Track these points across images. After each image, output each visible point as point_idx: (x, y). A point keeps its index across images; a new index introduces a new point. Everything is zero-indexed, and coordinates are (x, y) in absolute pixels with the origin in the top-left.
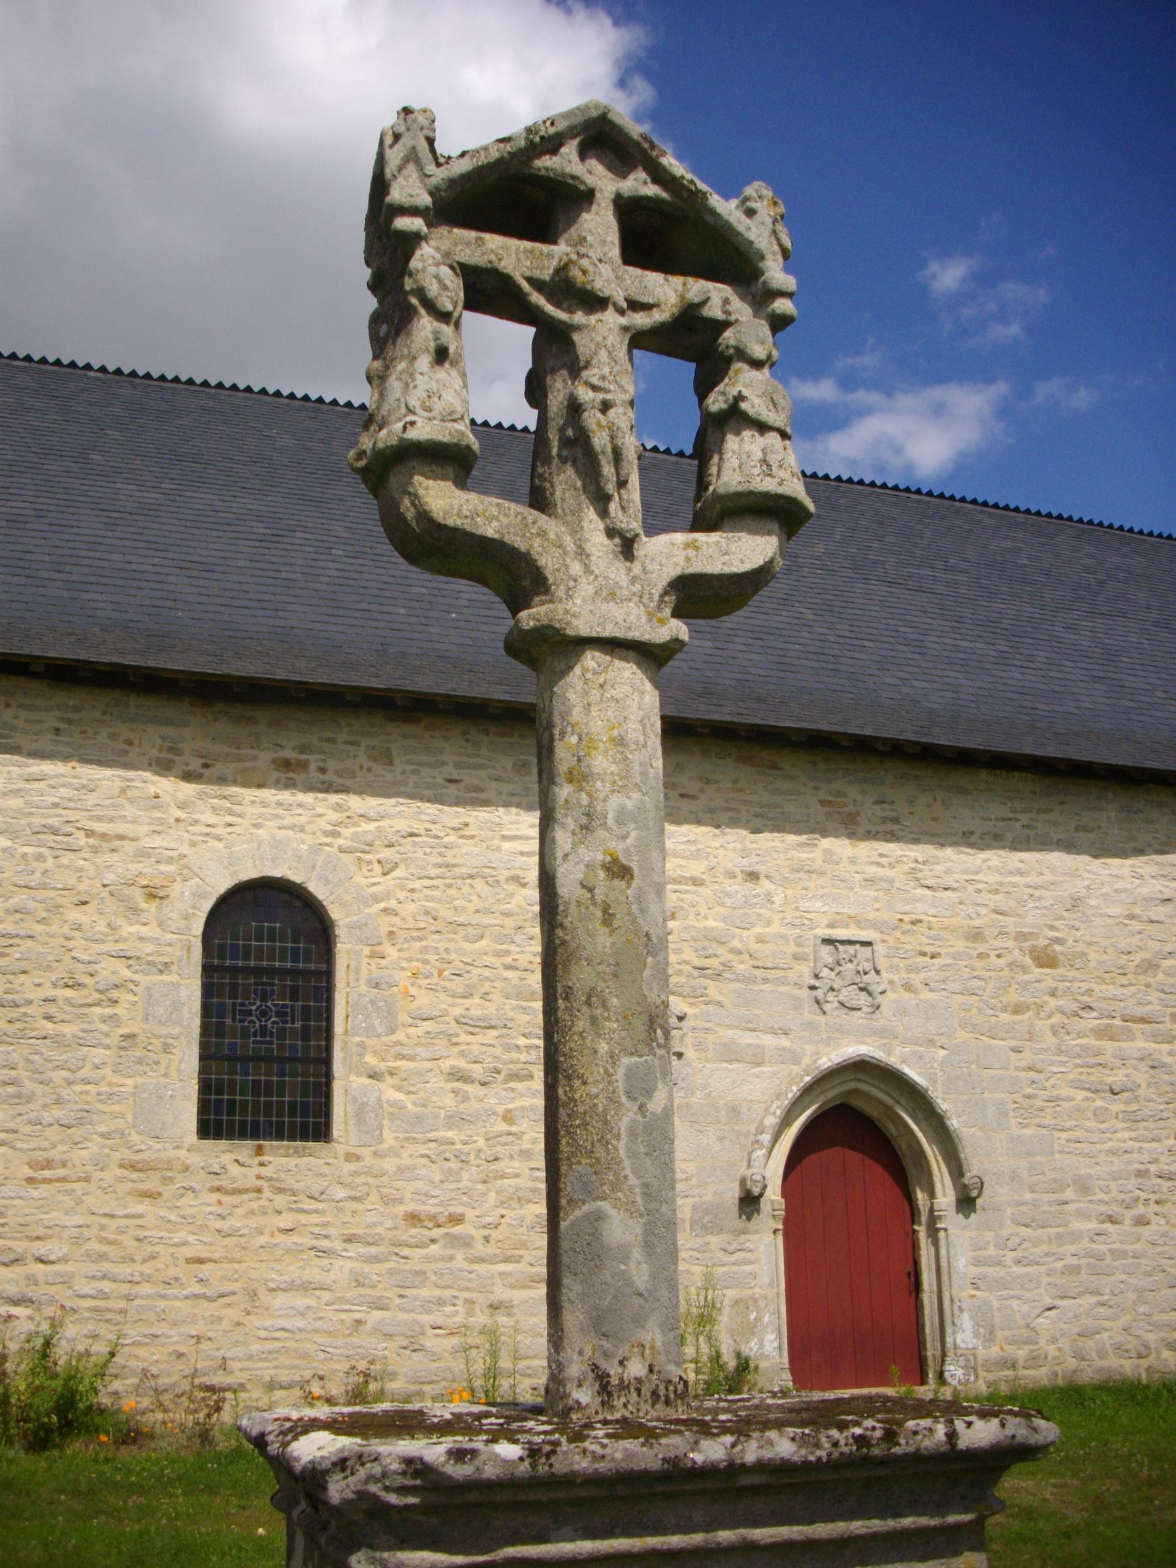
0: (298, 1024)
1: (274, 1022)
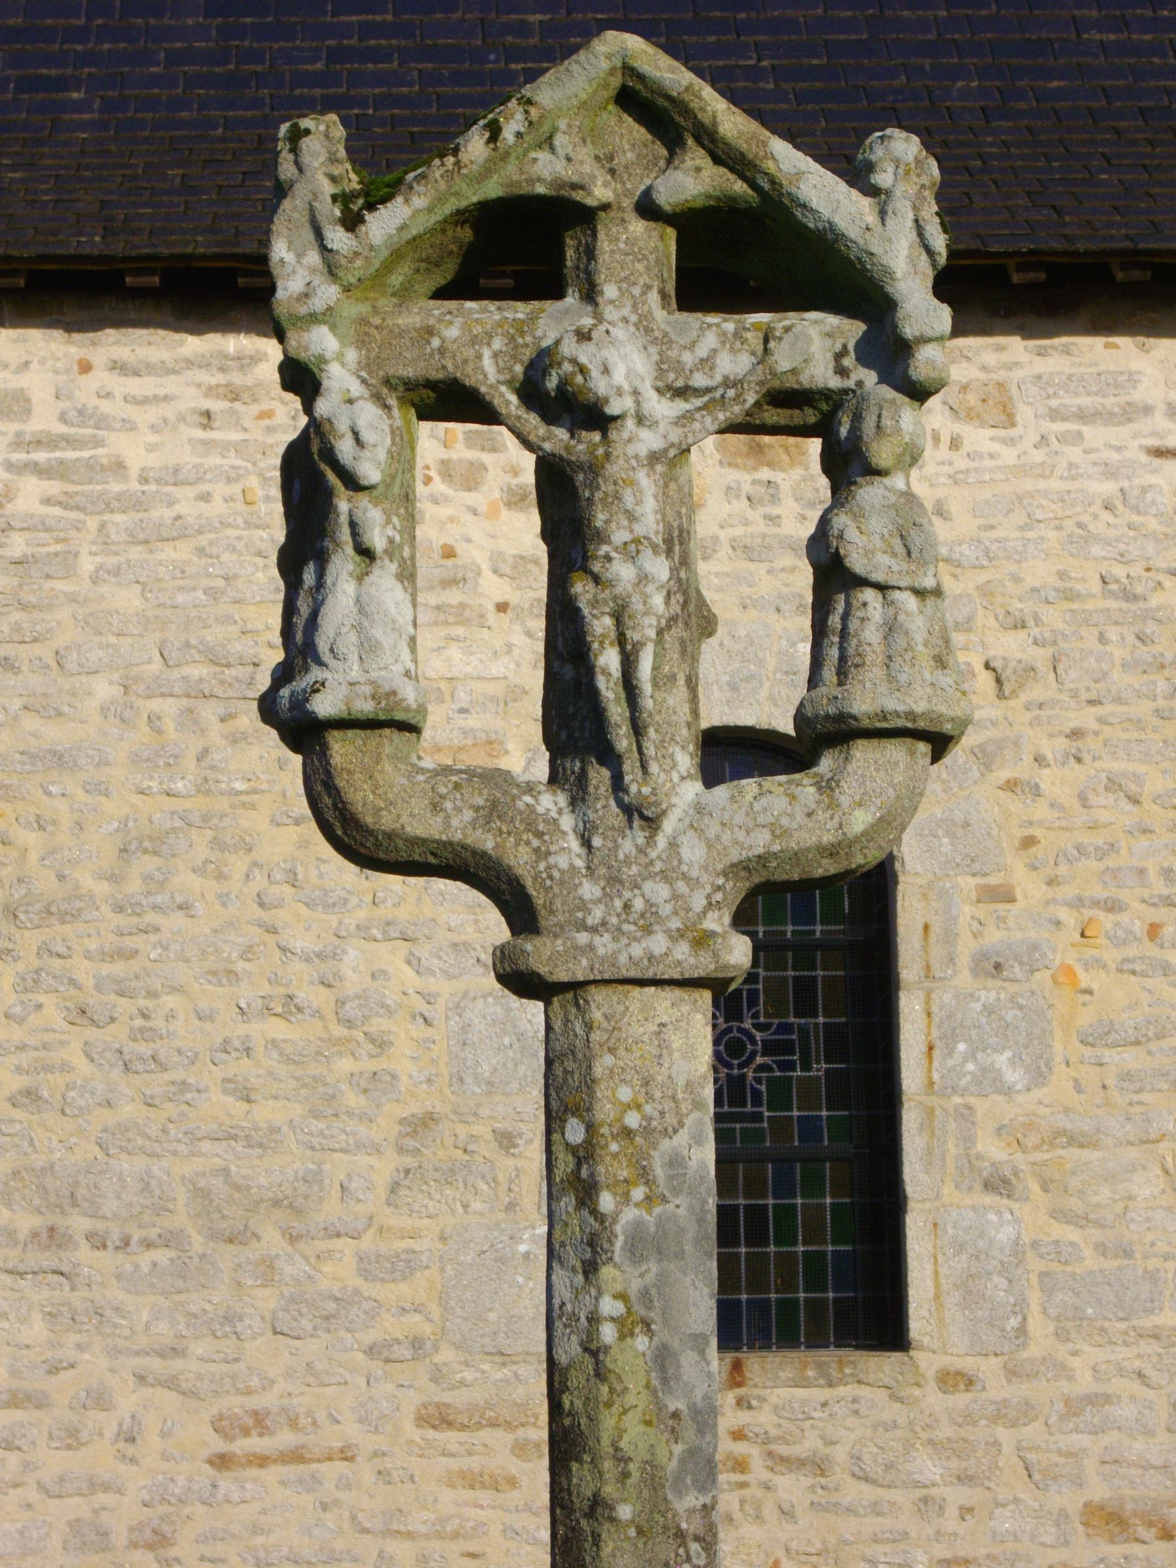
0: (820, 1069)
1: (761, 1068)
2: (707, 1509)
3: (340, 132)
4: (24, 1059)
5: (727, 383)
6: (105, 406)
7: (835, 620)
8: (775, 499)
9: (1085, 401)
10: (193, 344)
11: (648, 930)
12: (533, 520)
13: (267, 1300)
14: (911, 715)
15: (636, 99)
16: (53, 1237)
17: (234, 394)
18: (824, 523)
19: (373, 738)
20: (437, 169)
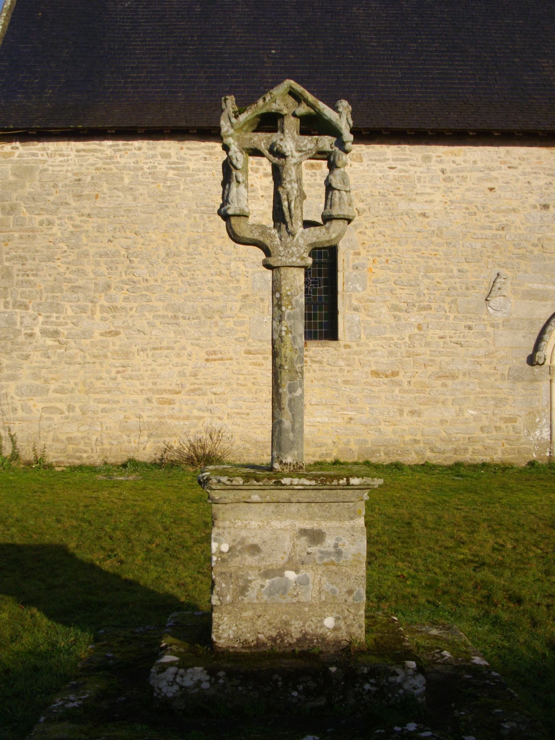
0: (322, 287)
2: (302, 367)
3: (234, 99)
4: (170, 283)
5: (309, 150)
6: (186, 156)
7: (329, 196)
8: (316, 176)
9: (376, 158)
10: (203, 144)
11: (292, 256)
12: (271, 178)
13: (216, 329)
14: (344, 215)
15: (292, 93)
16: (175, 317)
17: (211, 154)
18: (328, 177)
19: (239, 218)
20: (253, 107)
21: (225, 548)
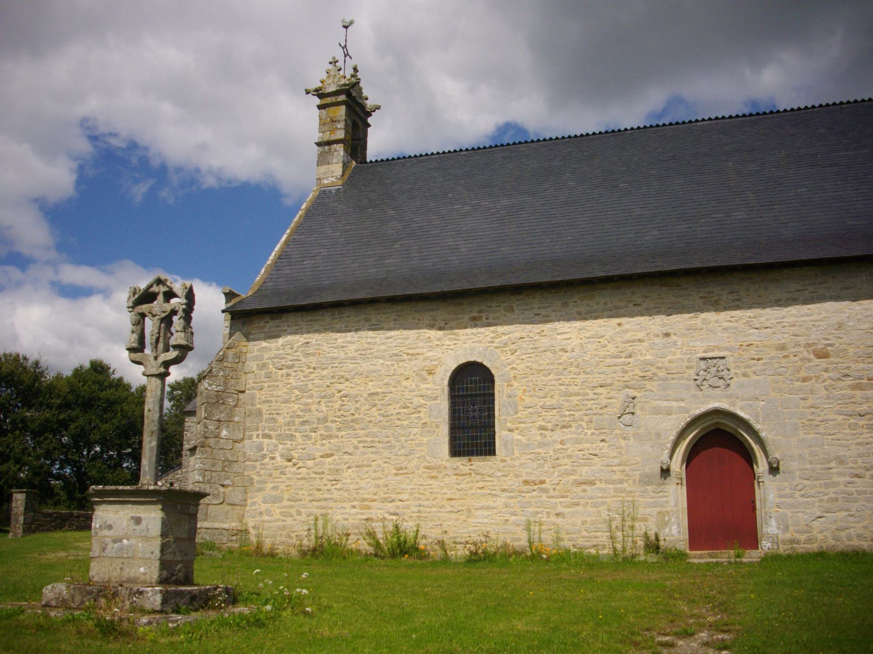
21: (98, 526)
